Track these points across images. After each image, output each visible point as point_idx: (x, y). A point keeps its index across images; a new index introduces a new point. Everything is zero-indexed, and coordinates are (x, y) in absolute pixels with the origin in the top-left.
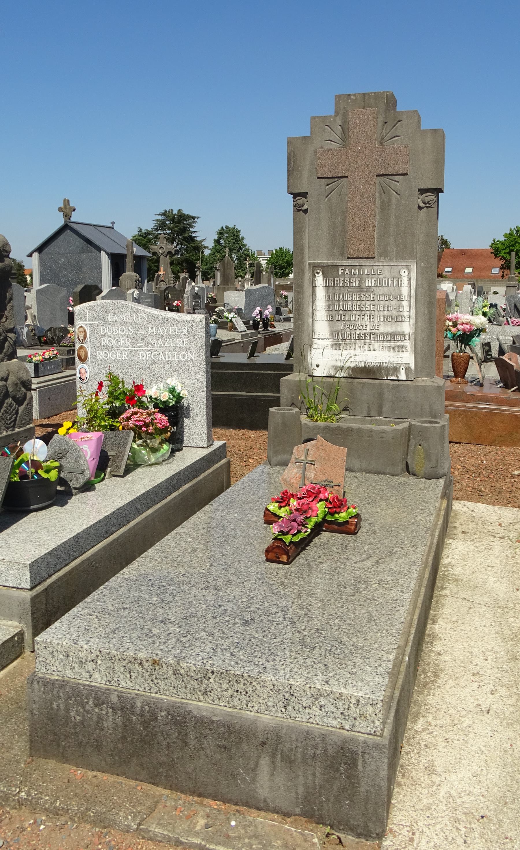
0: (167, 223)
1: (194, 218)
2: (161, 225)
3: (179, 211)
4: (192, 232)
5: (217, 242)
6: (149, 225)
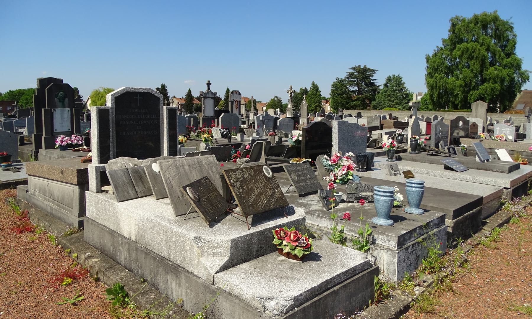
0: (356, 74)
1: (374, 71)
2: (351, 75)
3: (365, 66)
4: (372, 80)
5: (386, 85)
6: (343, 75)
